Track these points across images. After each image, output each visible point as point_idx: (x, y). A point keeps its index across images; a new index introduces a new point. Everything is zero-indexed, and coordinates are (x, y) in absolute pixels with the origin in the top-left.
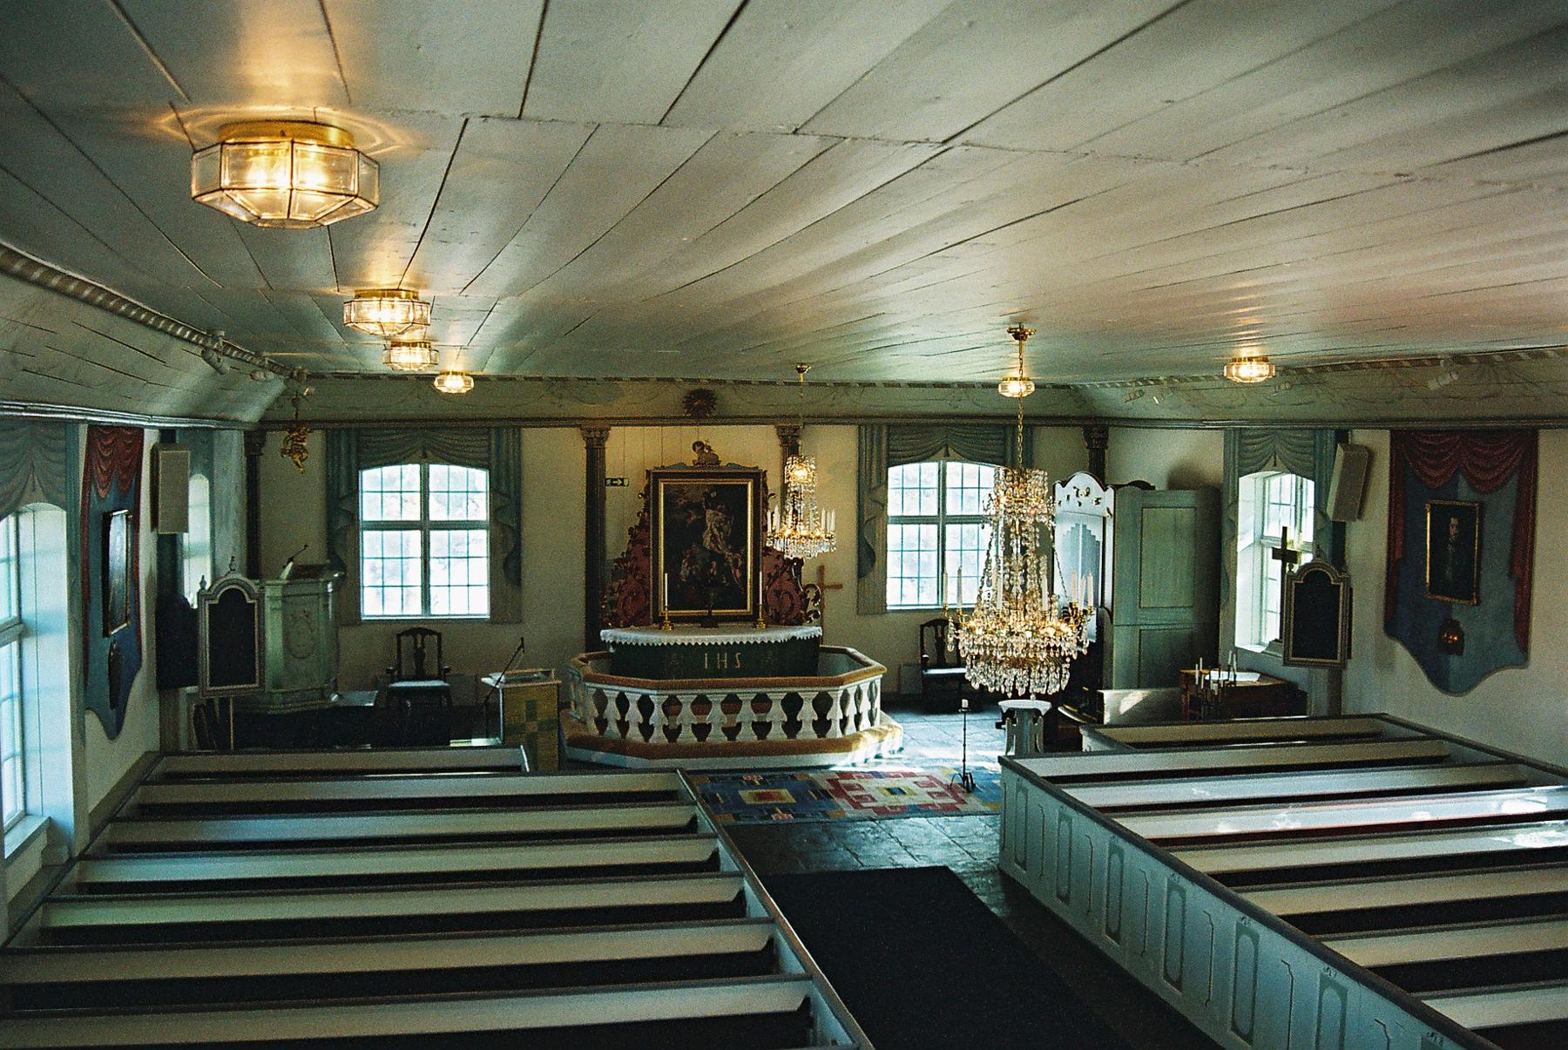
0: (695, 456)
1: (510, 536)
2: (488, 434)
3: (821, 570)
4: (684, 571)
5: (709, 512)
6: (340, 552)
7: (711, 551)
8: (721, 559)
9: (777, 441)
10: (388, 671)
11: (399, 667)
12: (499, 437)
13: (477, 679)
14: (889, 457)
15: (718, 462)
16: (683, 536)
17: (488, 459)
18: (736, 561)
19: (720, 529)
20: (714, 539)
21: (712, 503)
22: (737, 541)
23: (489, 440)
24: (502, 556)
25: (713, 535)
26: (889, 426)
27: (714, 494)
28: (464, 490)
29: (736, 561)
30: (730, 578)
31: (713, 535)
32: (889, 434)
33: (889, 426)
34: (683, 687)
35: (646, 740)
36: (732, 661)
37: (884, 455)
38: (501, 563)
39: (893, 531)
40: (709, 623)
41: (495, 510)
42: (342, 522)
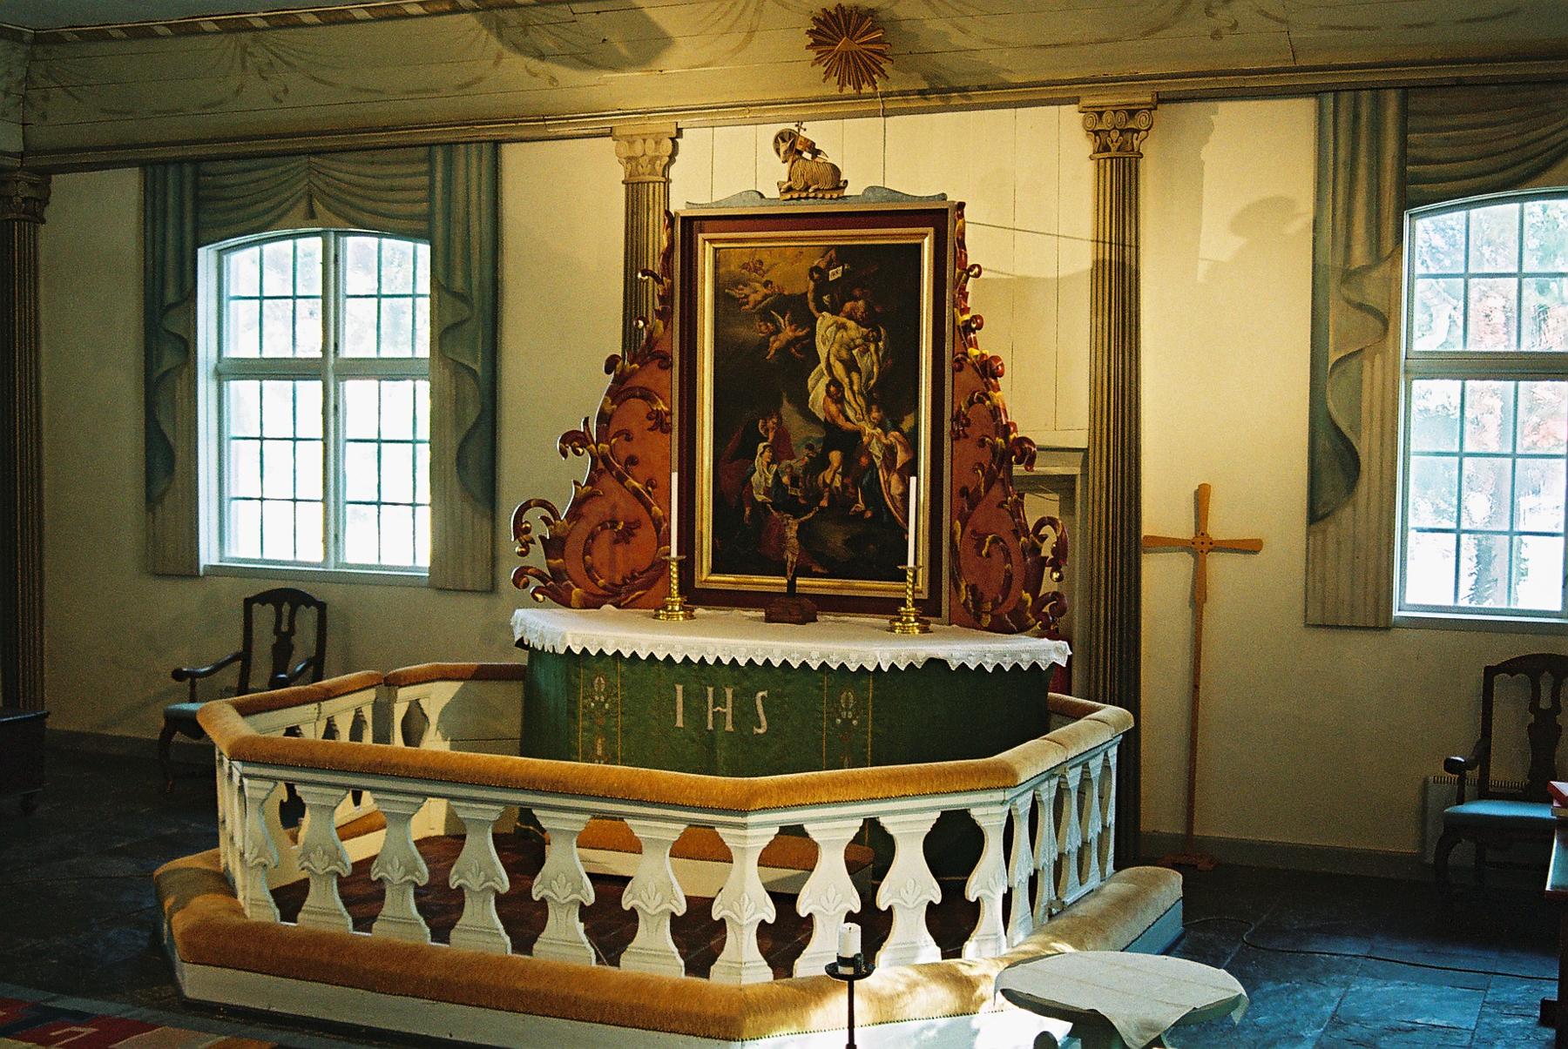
0: (782, 171)
1: (469, 388)
2: (430, 159)
3: (1201, 497)
4: (762, 474)
5: (825, 322)
6: (166, 427)
7: (829, 426)
8: (850, 442)
9: (1087, 146)
10: (1450, 766)
11: (1482, 754)
12: (449, 163)
13: (1547, 783)
14: (1403, 180)
15: (838, 184)
16: (760, 382)
17: (429, 217)
18: (890, 452)
19: (850, 365)
20: (836, 392)
21: (832, 296)
22: (893, 395)
23: (431, 173)
24: (452, 443)
25: (834, 382)
26: (1406, 90)
27: (835, 274)
28: (388, 289)
29: (890, 452)
30: (874, 494)
31: (834, 382)
32: (1404, 114)
33: (1406, 90)
34: (556, 787)
35: (363, 923)
36: (745, 714)
37: (1389, 179)
38: (451, 455)
39: (1431, 398)
40: (792, 610)
41: (443, 334)
42: (169, 359)
